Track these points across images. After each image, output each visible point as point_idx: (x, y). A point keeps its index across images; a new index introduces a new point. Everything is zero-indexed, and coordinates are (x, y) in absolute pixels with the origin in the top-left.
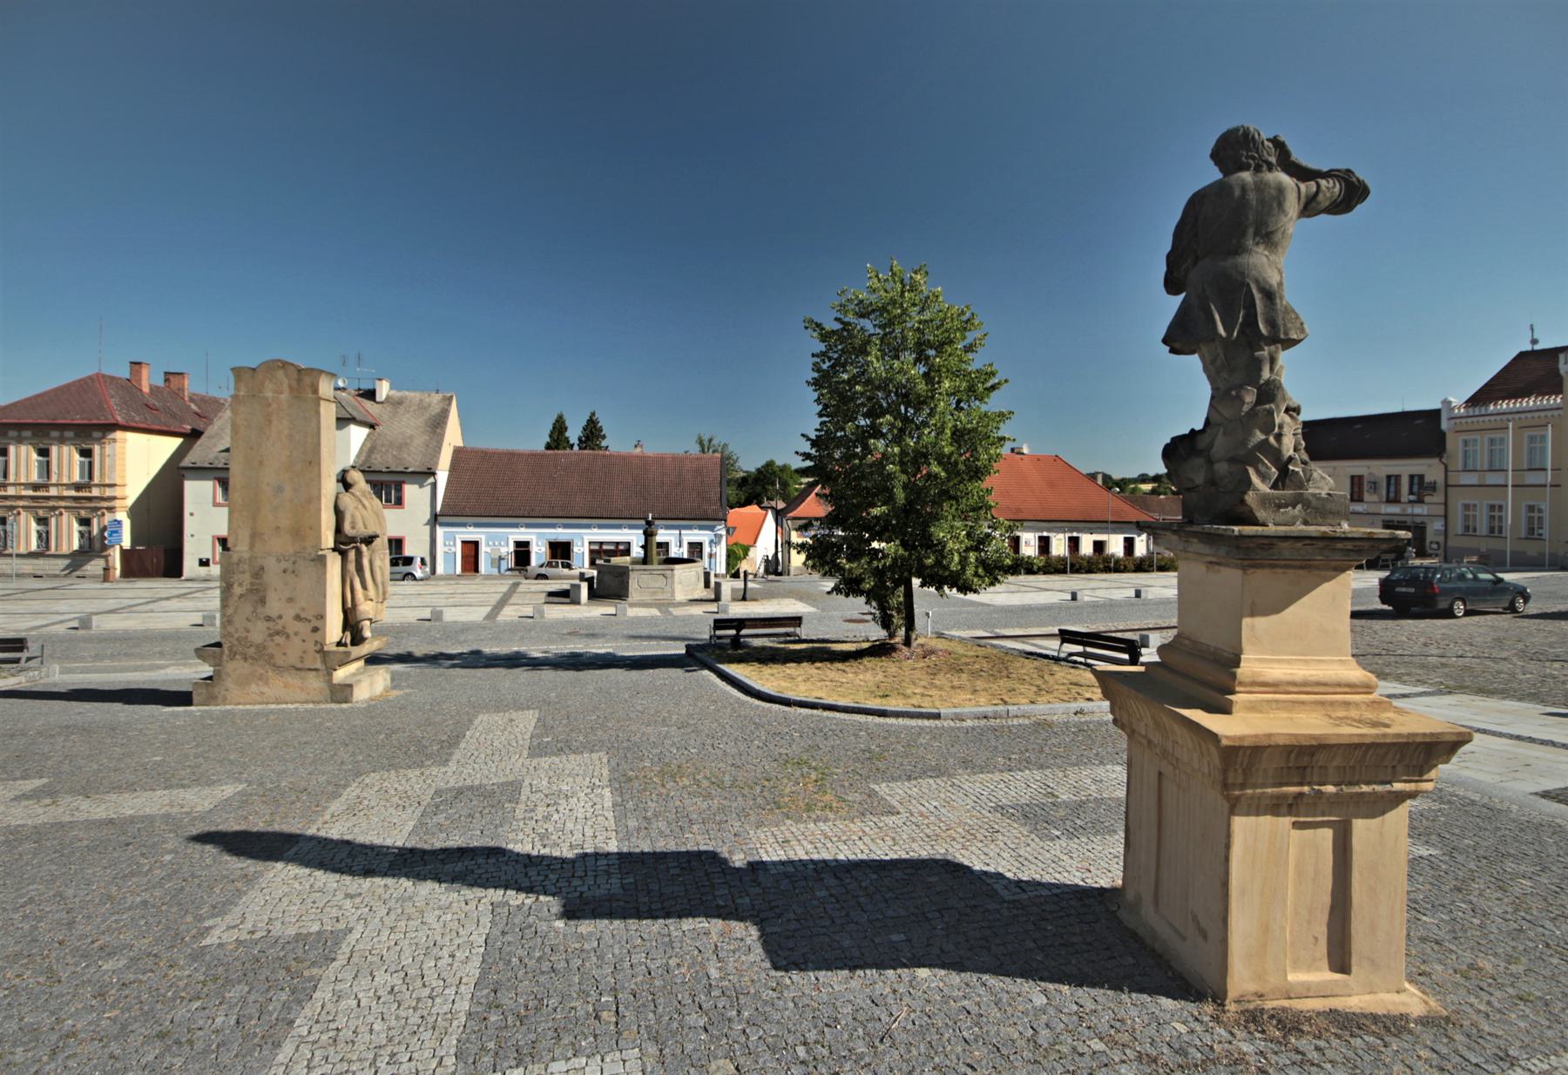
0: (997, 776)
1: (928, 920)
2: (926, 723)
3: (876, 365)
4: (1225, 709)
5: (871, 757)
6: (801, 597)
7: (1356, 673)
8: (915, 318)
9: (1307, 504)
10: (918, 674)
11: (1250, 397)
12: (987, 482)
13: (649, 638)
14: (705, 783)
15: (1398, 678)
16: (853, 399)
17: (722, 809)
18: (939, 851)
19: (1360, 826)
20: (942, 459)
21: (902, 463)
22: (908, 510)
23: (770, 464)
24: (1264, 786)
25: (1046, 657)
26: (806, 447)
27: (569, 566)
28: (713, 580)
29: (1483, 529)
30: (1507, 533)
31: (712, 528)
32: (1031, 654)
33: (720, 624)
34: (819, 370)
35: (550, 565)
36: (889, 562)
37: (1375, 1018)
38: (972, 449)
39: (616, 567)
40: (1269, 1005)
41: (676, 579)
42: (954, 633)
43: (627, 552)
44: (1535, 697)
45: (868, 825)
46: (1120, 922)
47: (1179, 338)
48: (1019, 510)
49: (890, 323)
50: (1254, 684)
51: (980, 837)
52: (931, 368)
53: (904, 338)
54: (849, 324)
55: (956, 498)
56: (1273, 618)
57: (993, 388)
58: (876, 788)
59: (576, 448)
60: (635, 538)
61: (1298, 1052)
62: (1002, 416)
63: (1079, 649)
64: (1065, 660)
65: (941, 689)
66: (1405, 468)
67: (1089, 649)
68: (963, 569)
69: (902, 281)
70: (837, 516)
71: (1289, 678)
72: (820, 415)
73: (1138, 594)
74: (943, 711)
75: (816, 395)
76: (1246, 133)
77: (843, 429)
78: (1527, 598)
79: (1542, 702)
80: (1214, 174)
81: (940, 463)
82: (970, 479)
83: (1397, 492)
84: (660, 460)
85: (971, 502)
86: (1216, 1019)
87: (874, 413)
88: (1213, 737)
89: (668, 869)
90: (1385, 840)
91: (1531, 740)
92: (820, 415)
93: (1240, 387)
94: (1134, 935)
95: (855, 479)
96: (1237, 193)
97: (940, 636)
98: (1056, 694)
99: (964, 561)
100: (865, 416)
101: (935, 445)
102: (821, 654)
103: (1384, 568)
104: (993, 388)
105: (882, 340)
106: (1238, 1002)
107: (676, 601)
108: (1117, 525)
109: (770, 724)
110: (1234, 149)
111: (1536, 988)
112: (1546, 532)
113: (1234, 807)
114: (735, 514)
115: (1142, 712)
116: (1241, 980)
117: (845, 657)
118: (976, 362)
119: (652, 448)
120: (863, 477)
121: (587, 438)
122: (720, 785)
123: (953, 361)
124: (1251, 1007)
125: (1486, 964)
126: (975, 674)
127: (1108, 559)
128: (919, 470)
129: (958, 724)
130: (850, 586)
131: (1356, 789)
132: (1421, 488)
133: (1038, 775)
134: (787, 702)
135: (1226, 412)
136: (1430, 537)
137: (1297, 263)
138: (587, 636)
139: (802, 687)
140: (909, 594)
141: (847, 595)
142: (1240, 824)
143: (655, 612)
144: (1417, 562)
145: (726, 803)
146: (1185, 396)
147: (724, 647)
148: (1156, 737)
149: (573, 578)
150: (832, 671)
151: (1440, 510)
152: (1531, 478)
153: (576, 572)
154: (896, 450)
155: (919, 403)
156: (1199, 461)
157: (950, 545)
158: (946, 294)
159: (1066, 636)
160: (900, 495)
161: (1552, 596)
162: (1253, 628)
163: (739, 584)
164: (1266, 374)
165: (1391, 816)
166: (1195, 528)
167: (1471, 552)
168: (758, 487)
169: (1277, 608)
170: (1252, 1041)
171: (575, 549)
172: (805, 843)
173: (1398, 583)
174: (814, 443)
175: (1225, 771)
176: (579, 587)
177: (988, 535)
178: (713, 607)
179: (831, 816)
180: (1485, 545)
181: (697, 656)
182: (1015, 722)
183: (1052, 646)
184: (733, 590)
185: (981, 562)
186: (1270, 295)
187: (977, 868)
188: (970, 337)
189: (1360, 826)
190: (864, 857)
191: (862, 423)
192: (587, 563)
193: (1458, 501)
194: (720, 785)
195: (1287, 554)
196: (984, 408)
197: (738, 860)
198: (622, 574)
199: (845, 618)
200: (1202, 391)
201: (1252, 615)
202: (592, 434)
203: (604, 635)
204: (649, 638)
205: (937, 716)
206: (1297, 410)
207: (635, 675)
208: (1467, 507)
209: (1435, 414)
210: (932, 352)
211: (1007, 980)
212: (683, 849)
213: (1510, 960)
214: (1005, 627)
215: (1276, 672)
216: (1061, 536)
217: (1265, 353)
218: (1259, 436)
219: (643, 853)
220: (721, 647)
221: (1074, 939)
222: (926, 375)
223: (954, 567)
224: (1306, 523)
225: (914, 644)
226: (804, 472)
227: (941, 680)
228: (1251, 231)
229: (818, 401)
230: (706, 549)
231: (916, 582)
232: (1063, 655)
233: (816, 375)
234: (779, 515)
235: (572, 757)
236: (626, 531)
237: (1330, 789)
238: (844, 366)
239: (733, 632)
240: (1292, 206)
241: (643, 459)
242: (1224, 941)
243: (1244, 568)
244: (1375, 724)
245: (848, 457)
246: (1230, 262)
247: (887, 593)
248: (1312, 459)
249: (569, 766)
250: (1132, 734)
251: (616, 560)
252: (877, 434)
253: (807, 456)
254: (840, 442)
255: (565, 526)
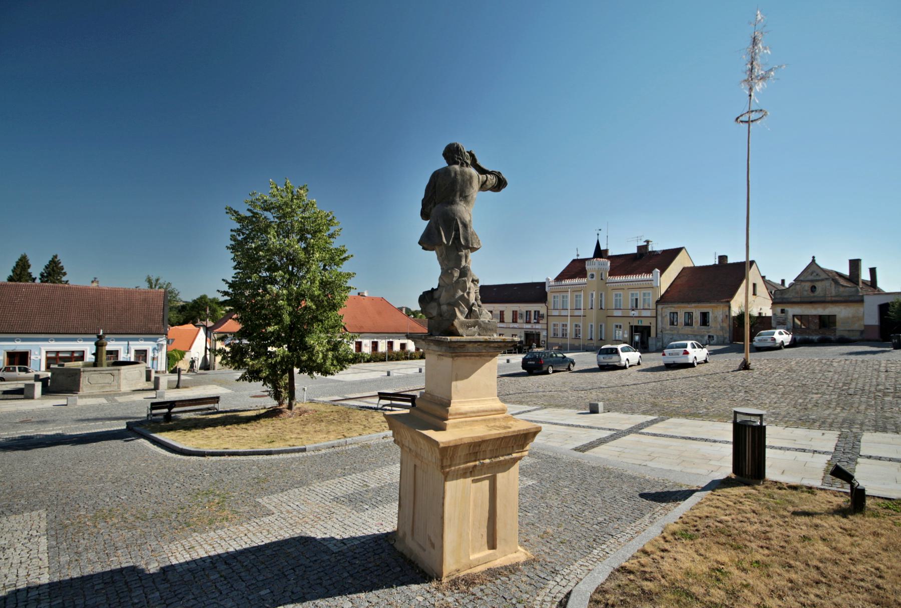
0: (337, 480)
1: (286, 576)
2: (297, 455)
3: (274, 241)
4: (442, 428)
5: (258, 481)
6: (221, 384)
7: (498, 404)
8: (298, 217)
9: (480, 326)
10: (295, 426)
11: (456, 274)
12: (340, 312)
13: (96, 419)
14: (132, 519)
15: (527, 404)
16: (258, 259)
17: (144, 535)
18: (297, 532)
19: (500, 477)
20: (313, 298)
21: (288, 300)
22: (292, 327)
23: (203, 298)
24: (460, 464)
25: (371, 408)
26: (226, 288)
27: (26, 370)
28: (153, 375)
29: (560, 335)
30: (568, 336)
31: (155, 340)
32: (363, 407)
33: (155, 406)
34: (235, 240)
35: (7, 369)
36: (279, 359)
37: (506, 568)
38: (330, 295)
39: (69, 370)
40: (461, 574)
41: (122, 376)
42: (321, 399)
43: (81, 357)
44: (575, 407)
45: (252, 526)
46: (395, 549)
47: (428, 241)
48: (361, 327)
49: (284, 216)
50: (456, 414)
51: (323, 518)
52: (308, 245)
53: (292, 226)
54: (257, 214)
55: (321, 321)
56: (465, 381)
57: (345, 259)
58: (260, 500)
59: (38, 281)
60: (88, 348)
61: (473, 594)
62: (349, 275)
63: (388, 402)
64: (381, 409)
65: (308, 433)
66: (533, 307)
67: (394, 402)
68: (325, 361)
69: (292, 193)
70: (245, 331)
71: (472, 410)
72: (235, 268)
73: (389, 374)
74: (307, 447)
75: (232, 255)
76: (458, 147)
77: (250, 278)
78: (574, 364)
79: (577, 408)
80: (443, 163)
81: (312, 300)
82: (330, 310)
83: (530, 318)
84: (113, 292)
85: (330, 323)
86: (437, 589)
87: (273, 268)
88: (436, 443)
89: (93, 586)
90: (510, 481)
91: (573, 426)
92: (235, 268)
93: (453, 268)
94: (402, 555)
95: (258, 308)
96: (453, 175)
97: (311, 401)
98: (374, 429)
99: (325, 357)
100: (267, 270)
101: (309, 290)
102: (233, 419)
103: (525, 353)
104: (345, 259)
105: (278, 225)
106: (448, 577)
107: (127, 391)
108: (398, 334)
109: (188, 470)
110: (452, 153)
111: (567, 536)
112: (581, 335)
113: (447, 477)
114: (173, 331)
115: (407, 434)
116: (450, 565)
117: (248, 420)
118: (335, 244)
119: (107, 283)
120: (263, 307)
121: (49, 274)
122: (144, 519)
123: (321, 242)
124: (454, 577)
125: (549, 530)
126: (330, 422)
127: (406, 353)
128: (299, 304)
129: (317, 453)
130: (253, 375)
131: (498, 459)
132: (539, 316)
133: (359, 475)
134: (203, 454)
135: (447, 281)
136: (542, 338)
137: (477, 211)
138: (39, 422)
139: (215, 443)
140: (292, 378)
141: (250, 381)
142: (452, 487)
143: (103, 401)
144: (536, 350)
145: (146, 530)
146: (427, 271)
147: (163, 418)
148: (413, 447)
149: (29, 379)
150: (237, 431)
151: (545, 327)
152: (577, 313)
153: (32, 375)
154: (285, 292)
155: (301, 265)
156: (434, 304)
157: (317, 348)
158: (320, 202)
159: (382, 396)
160: (287, 319)
161: (583, 363)
162: (456, 387)
163: (175, 377)
164: (463, 263)
165: (512, 469)
166: (432, 338)
167: (555, 345)
168: (193, 313)
169: (467, 377)
170: (452, 596)
171: (32, 357)
172: (205, 546)
173: (529, 360)
174: (231, 285)
175: (442, 460)
176: (33, 386)
177: (340, 342)
178: (152, 394)
179: (227, 524)
180: (561, 341)
181: (136, 429)
182: (350, 447)
183: (375, 402)
184: (169, 382)
185: (336, 358)
186: (465, 226)
187: (319, 537)
188: (332, 230)
189: (500, 477)
190: (247, 546)
191: (264, 274)
192: (43, 367)
193: (552, 322)
194: (144, 519)
195: (471, 350)
196: (339, 270)
197: (153, 568)
198: (76, 373)
199: (253, 395)
200: (437, 270)
201: (456, 380)
202: (54, 271)
203: (54, 421)
204: (96, 419)
205: (304, 450)
206: (477, 281)
207: (79, 448)
208: (554, 325)
209: (543, 285)
210: (309, 236)
211: (331, 599)
212: (108, 569)
213: (559, 526)
214: (351, 393)
215: (466, 407)
216: (384, 341)
217: (463, 253)
218: (460, 293)
219: (72, 579)
220: (157, 422)
221: (370, 565)
222: (304, 249)
223: (319, 361)
224: (479, 335)
225: (294, 408)
226: (224, 303)
227: (309, 428)
228: (458, 194)
229: (234, 259)
230: (150, 355)
231: (296, 370)
232: (380, 406)
233: (233, 243)
234: (208, 330)
235: (12, 518)
236: (81, 343)
237: (487, 461)
238: (253, 239)
239: (166, 410)
240: (476, 185)
241: (100, 292)
242: (442, 547)
243: (453, 357)
244: (505, 428)
245: (254, 296)
246: (449, 207)
247: (278, 378)
248: (483, 302)
249: (9, 525)
250: (402, 446)
251: (68, 365)
252: (273, 282)
253: (226, 293)
254: (248, 286)
255: (23, 340)
